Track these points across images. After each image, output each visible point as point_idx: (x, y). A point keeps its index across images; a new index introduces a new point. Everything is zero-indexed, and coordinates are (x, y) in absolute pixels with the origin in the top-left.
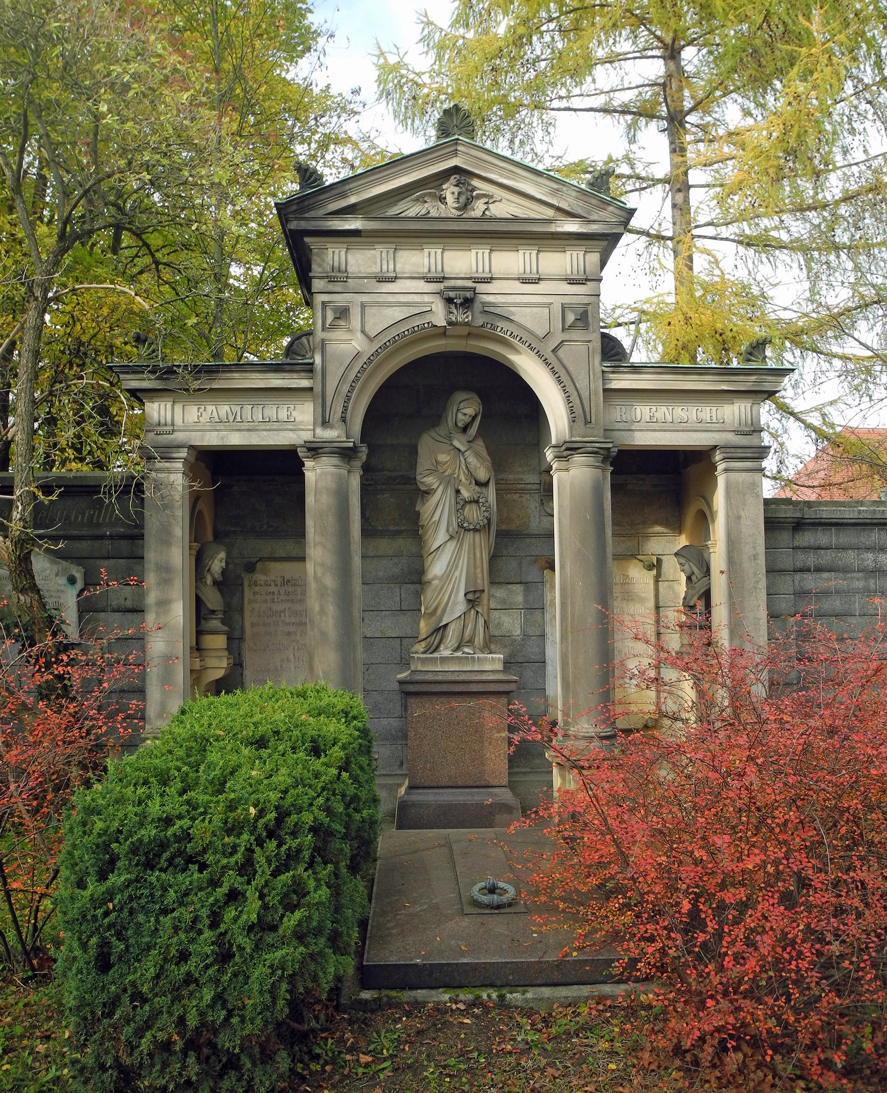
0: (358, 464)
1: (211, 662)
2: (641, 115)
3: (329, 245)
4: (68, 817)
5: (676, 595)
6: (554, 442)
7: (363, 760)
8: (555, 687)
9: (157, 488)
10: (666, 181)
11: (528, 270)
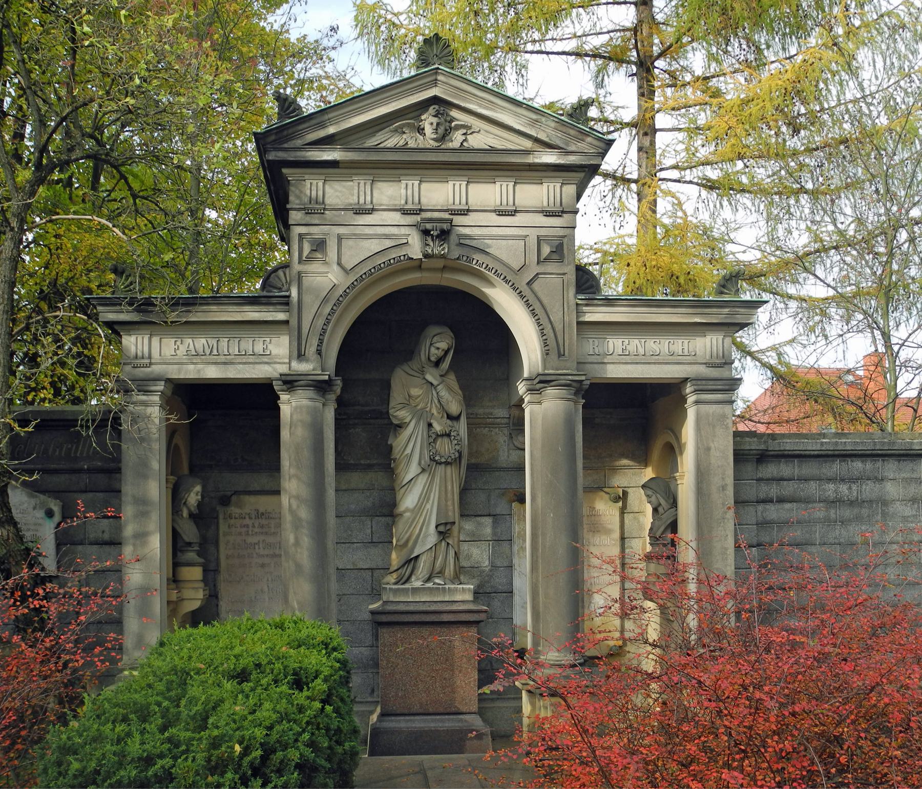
0: (332, 397)
1: (187, 593)
2: (610, 59)
3: (307, 177)
4: (42, 757)
5: (641, 528)
6: (526, 375)
7: (343, 691)
8: (523, 616)
9: (134, 421)
10: (633, 125)
11: (504, 202)
